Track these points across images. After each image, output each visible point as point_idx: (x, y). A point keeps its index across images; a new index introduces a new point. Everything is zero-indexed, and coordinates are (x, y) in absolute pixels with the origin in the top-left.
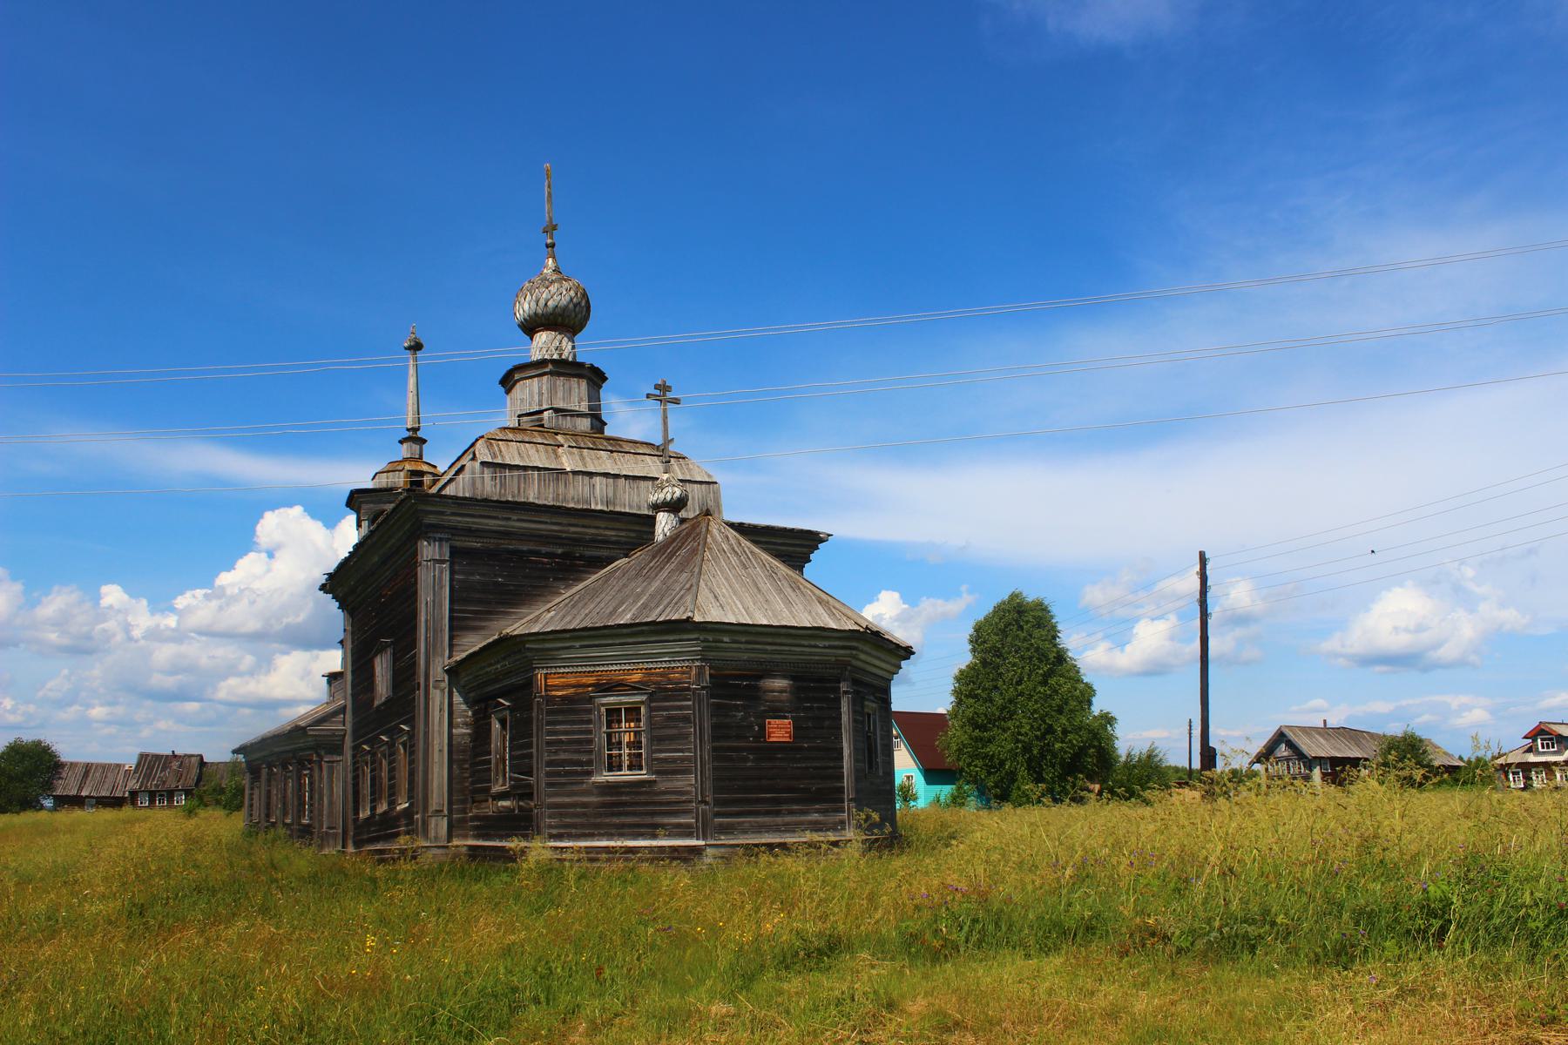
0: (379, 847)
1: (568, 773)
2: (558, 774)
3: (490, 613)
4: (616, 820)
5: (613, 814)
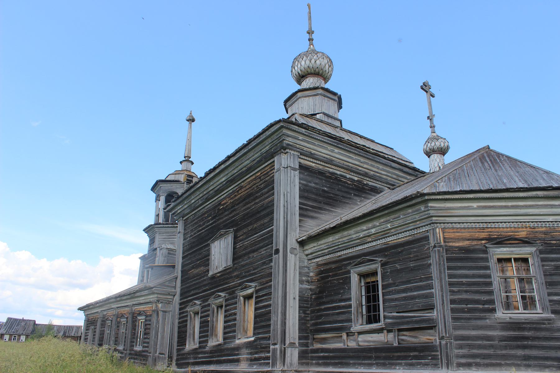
1: (470, 311)
2: (462, 311)
3: (320, 208)
4: (520, 352)
5: (518, 347)
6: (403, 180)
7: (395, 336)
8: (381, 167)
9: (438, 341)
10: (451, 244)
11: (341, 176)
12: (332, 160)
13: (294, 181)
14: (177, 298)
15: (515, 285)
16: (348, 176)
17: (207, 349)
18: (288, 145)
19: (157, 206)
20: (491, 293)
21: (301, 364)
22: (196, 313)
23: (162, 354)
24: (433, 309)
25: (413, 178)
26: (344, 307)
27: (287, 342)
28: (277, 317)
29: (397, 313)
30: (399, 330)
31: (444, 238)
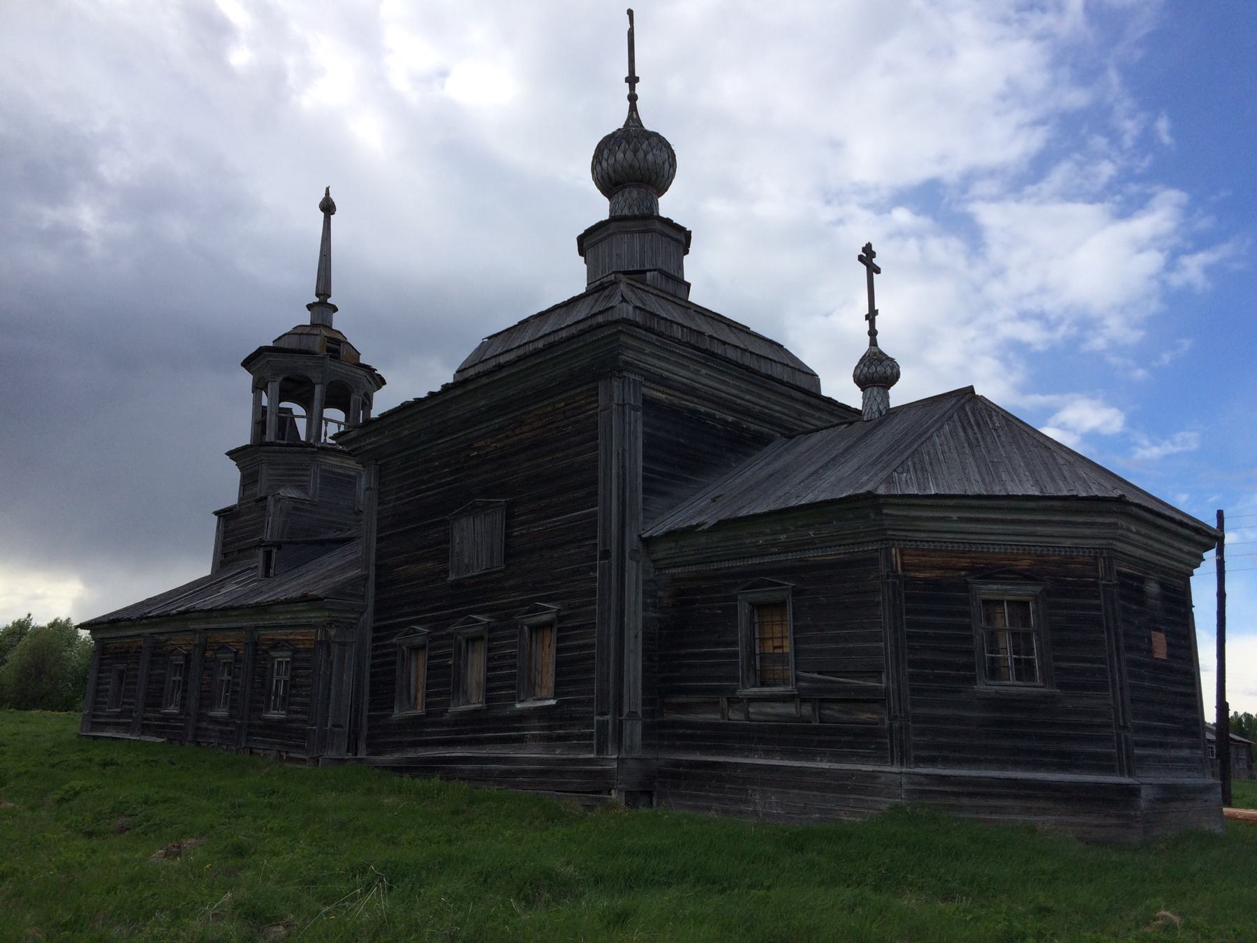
0: (397, 739)
6: (813, 421)
7: (814, 710)
8: (773, 398)
9: (887, 721)
10: (913, 574)
11: (707, 414)
12: (694, 389)
13: (635, 427)
14: (368, 618)
15: (1006, 642)
16: (718, 415)
17: (447, 717)
18: (626, 363)
19: (257, 400)
20: (970, 653)
21: (645, 746)
22: (416, 649)
23: (339, 726)
24: (880, 673)
25: (836, 421)
26: (722, 655)
27: (626, 710)
28: (608, 668)
29: (820, 673)
30: (822, 700)
31: (902, 564)
